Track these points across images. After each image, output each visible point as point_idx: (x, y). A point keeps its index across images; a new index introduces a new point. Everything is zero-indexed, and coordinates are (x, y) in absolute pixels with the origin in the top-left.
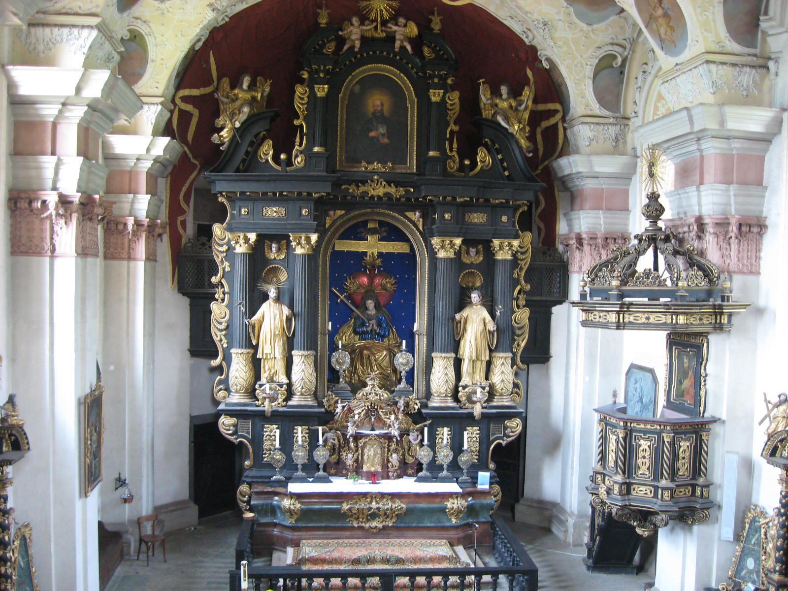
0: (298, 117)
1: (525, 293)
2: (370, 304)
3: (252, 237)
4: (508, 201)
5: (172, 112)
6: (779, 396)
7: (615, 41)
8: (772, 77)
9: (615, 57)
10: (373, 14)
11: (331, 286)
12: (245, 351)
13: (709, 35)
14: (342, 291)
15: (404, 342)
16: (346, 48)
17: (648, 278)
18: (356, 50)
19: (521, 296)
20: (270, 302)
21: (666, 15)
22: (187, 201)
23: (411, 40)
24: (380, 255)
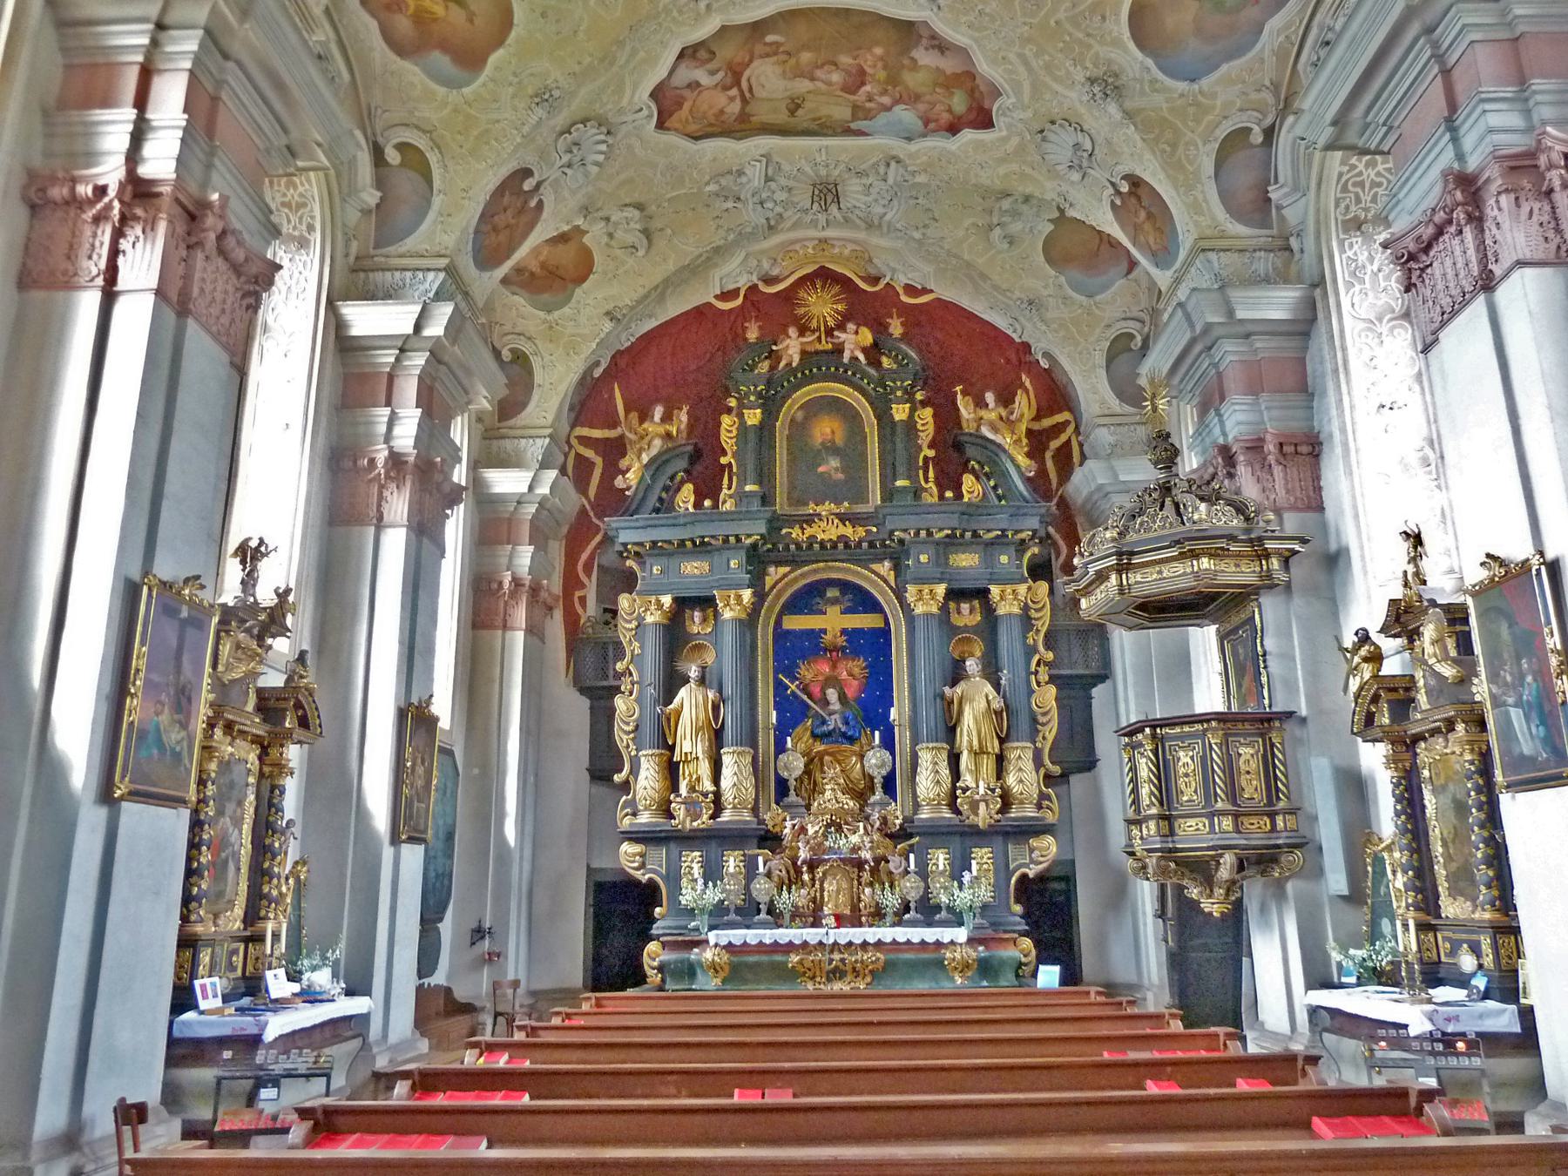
0: (724, 453)
1: (1046, 664)
2: (832, 695)
3: (667, 600)
4: (1004, 535)
5: (566, 456)
6: (1356, 634)
7: (1128, 315)
8: (1297, 256)
9: (1131, 337)
10: (815, 321)
11: (776, 673)
12: (657, 751)
13: (1202, 218)
14: (793, 679)
15: (877, 733)
16: (782, 364)
17: (1155, 522)
18: (794, 365)
19: (1042, 669)
20: (692, 684)
21: (1150, 216)
22: (588, 573)
23: (864, 350)
24: (844, 632)
